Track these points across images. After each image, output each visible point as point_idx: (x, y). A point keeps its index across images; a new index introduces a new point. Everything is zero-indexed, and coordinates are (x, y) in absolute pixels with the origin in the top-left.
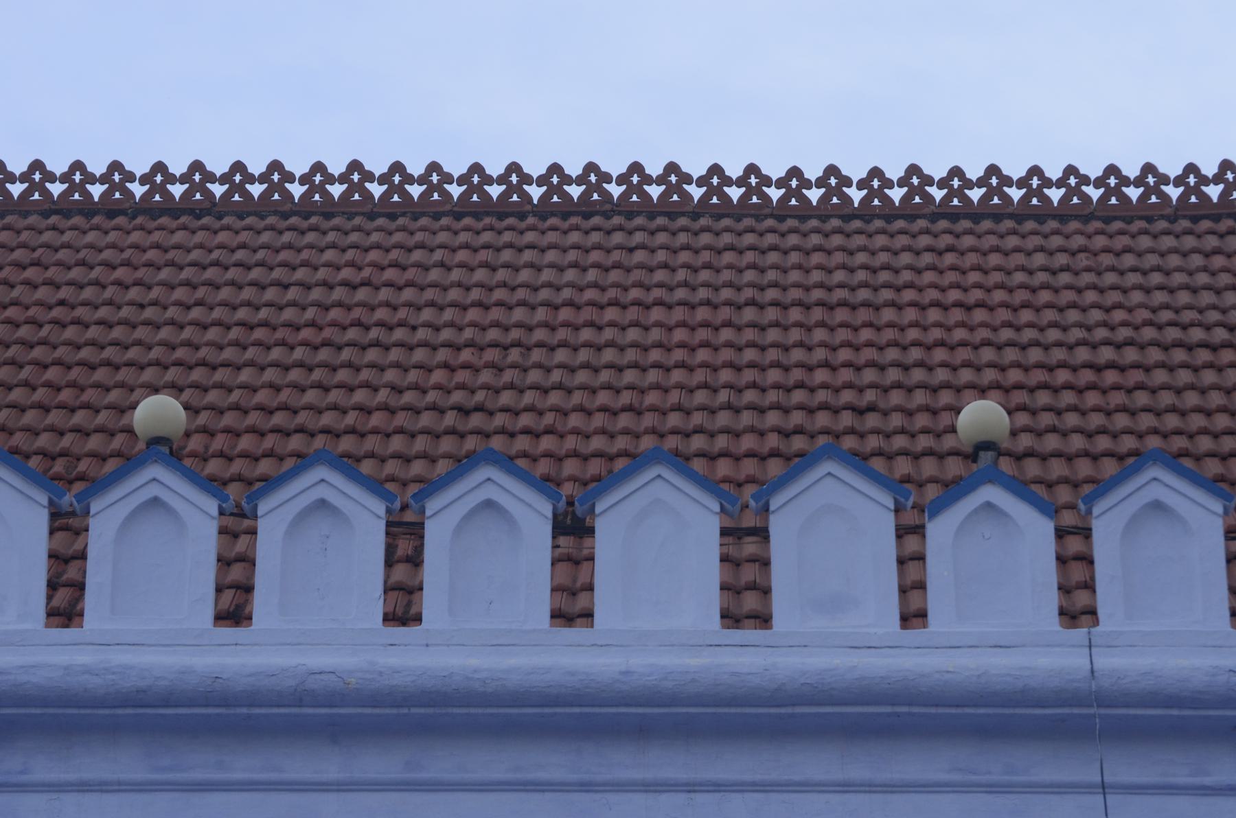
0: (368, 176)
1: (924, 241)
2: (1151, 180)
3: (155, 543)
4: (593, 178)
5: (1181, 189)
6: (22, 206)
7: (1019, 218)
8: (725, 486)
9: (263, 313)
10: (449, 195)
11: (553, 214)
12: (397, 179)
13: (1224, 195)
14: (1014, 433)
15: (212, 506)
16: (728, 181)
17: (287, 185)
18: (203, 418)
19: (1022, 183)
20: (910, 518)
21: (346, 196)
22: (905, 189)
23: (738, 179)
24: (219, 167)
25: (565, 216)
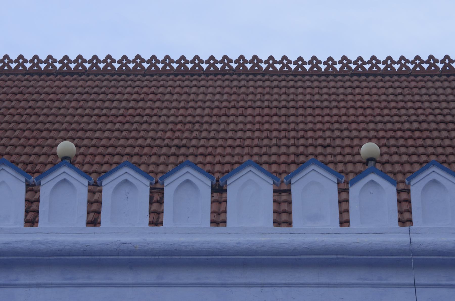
0: (114, 61)
1: (348, 84)
3: (65, 196)
5: (326, 66)
7: (383, 75)
8: (275, 175)
9: (104, 111)
14: (381, 155)
15: (85, 182)
16: (276, 62)
17: (113, 64)
19: (384, 62)
20: (343, 186)
22: (341, 65)
23: (280, 61)
25: (216, 75)
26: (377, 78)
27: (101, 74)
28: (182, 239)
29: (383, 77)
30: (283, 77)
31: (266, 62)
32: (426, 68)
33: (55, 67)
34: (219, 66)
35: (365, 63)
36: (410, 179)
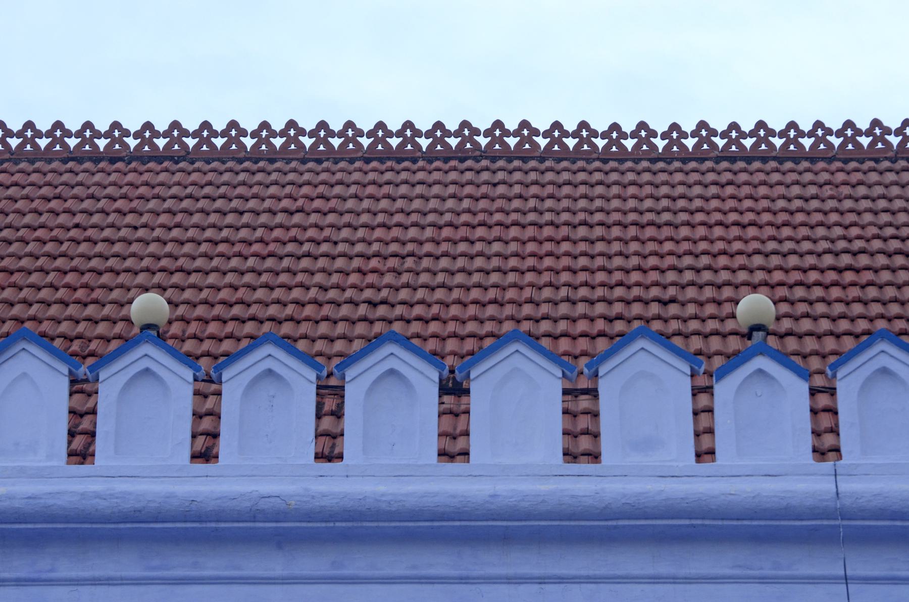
1: (711, 177)
2: (878, 131)
3: (148, 403)
4: (466, 132)
6: (16, 156)
8: (566, 358)
10: (361, 145)
11: (437, 159)
12: (498, 133)
13: (902, 144)
14: (778, 319)
16: (448, 134)
18: (181, 310)
21: (285, 146)
22: (697, 139)
23: (574, 132)
24: (778, 125)
26: (767, 165)
27: (90, 159)
28: (410, 488)
29: (781, 163)
30: (580, 164)
31: (546, 134)
32: (778, 146)
33: (360, 145)
34: (453, 142)
35: (743, 135)
36: (835, 367)
